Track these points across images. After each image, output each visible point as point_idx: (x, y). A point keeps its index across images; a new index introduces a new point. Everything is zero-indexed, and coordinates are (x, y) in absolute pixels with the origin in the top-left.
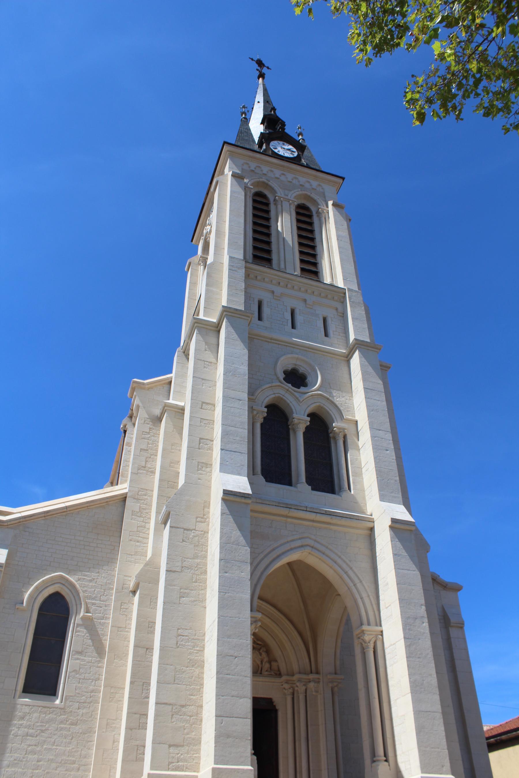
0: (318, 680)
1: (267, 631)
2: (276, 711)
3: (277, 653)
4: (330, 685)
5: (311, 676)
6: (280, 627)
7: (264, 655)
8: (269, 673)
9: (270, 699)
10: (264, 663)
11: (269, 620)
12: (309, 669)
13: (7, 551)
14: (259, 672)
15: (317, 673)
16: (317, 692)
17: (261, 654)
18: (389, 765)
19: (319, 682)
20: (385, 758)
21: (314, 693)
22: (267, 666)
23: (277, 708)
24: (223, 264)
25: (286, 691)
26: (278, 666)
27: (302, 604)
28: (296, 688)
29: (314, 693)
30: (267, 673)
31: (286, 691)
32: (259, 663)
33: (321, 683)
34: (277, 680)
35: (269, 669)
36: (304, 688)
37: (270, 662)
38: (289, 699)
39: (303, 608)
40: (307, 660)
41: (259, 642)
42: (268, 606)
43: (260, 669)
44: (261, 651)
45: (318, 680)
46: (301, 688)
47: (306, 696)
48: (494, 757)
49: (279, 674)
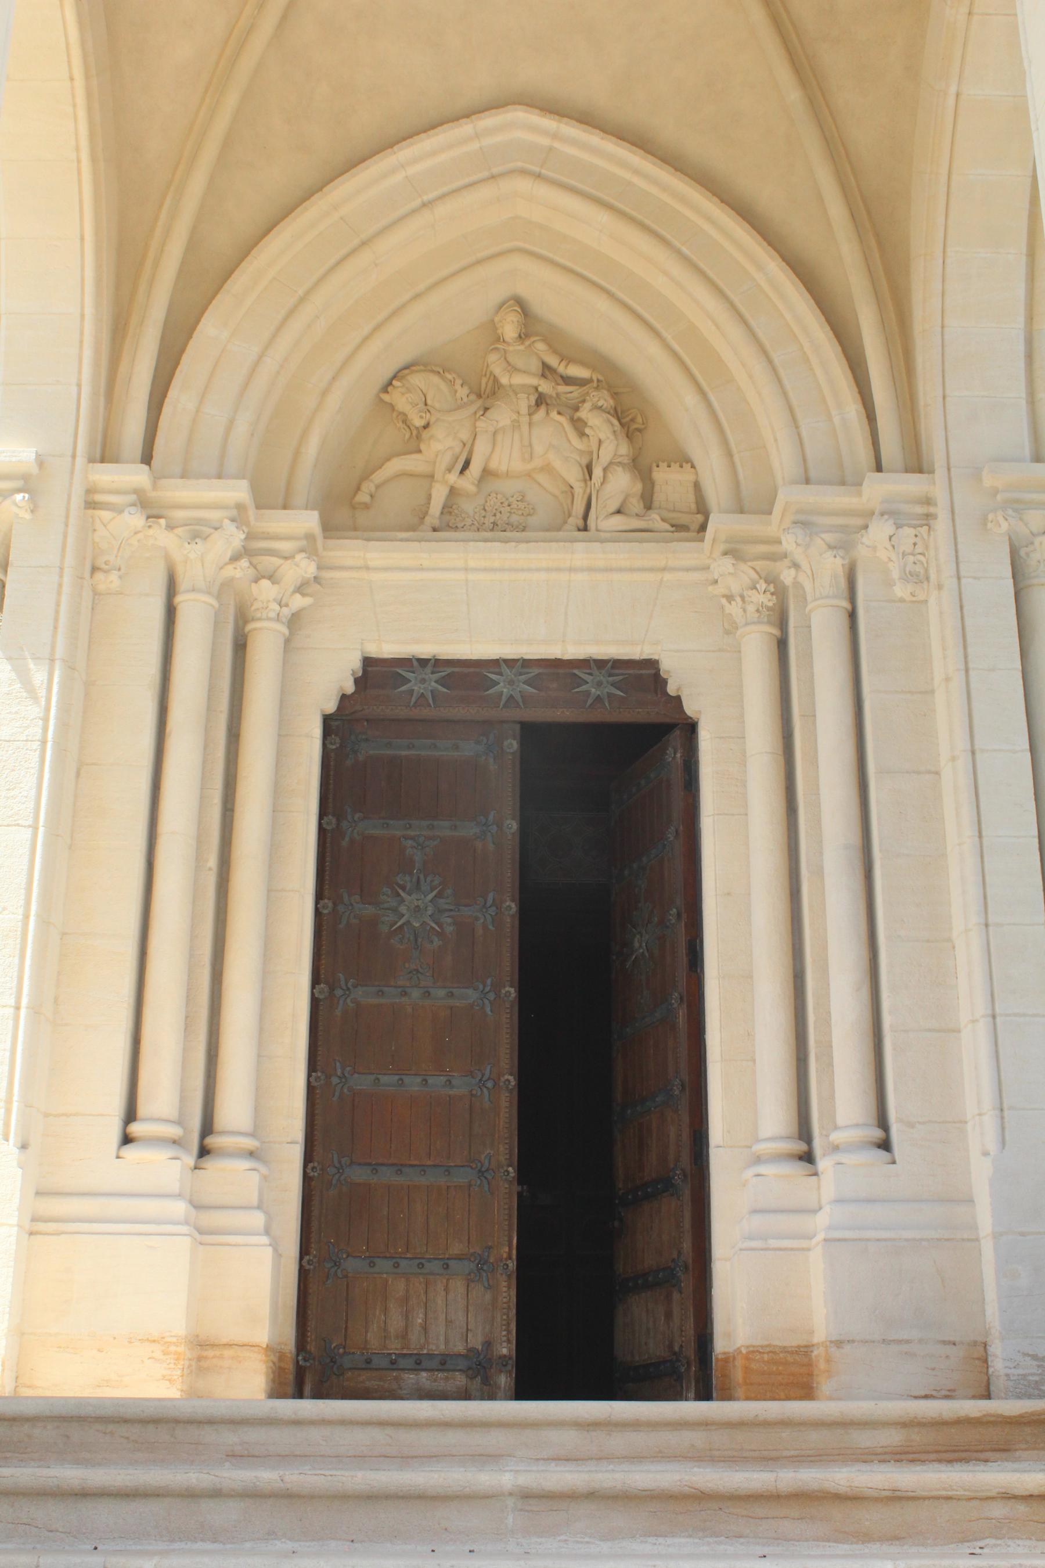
0: (919, 510)
2: (691, 728)
4: (1002, 526)
5: (878, 489)
9: (652, 664)
13: (245, 481)
14: (576, 520)
15: (917, 463)
17: (579, 427)
21: (900, 590)
22: (621, 484)
23: (690, 708)
25: (734, 609)
26: (697, 486)
27: (785, 75)
28: (787, 576)
29: (900, 590)
31: (734, 609)
32: (573, 475)
33: (942, 525)
34: (685, 553)
36: (832, 565)
37: (641, 468)
38: (755, 648)
39: (794, 96)
40: (853, 410)
42: (595, 139)
43: (579, 507)
44: (583, 413)
45: (919, 510)
46: (816, 573)
49: (693, 523)
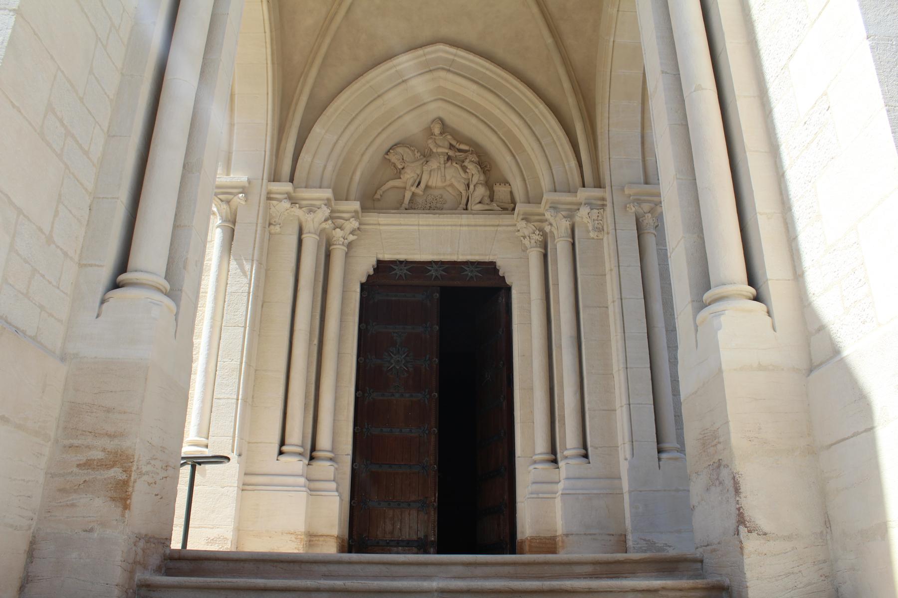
0: (600, 203)
1: (496, 133)
2: (509, 289)
3: (504, 162)
4: (632, 209)
5: (583, 194)
6: (504, 101)
7: (472, 168)
8: (487, 207)
9: (493, 264)
10: (472, 187)
11: (474, 87)
12: (577, 179)
14: (463, 205)
16: (600, 230)
17: (464, 169)
18: (769, 313)
19: (604, 206)
20: (752, 290)
23: (508, 281)
24: (663, 72)
26: (511, 193)
28: (547, 229)
30: (479, 207)
31: (526, 242)
33: (609, 209)
34: (506, 219)
35: (487, 200)
36: (565, 224)
37: (489, 185)
39: (550, 41)
40: (573, 163)
41: (463, 147)
43: (464, 201)
44: (466, 164)
45: (600, 203)
46: (559, 227)
47: (573, 244)
48: (188, 548)
49: (509, 207)
